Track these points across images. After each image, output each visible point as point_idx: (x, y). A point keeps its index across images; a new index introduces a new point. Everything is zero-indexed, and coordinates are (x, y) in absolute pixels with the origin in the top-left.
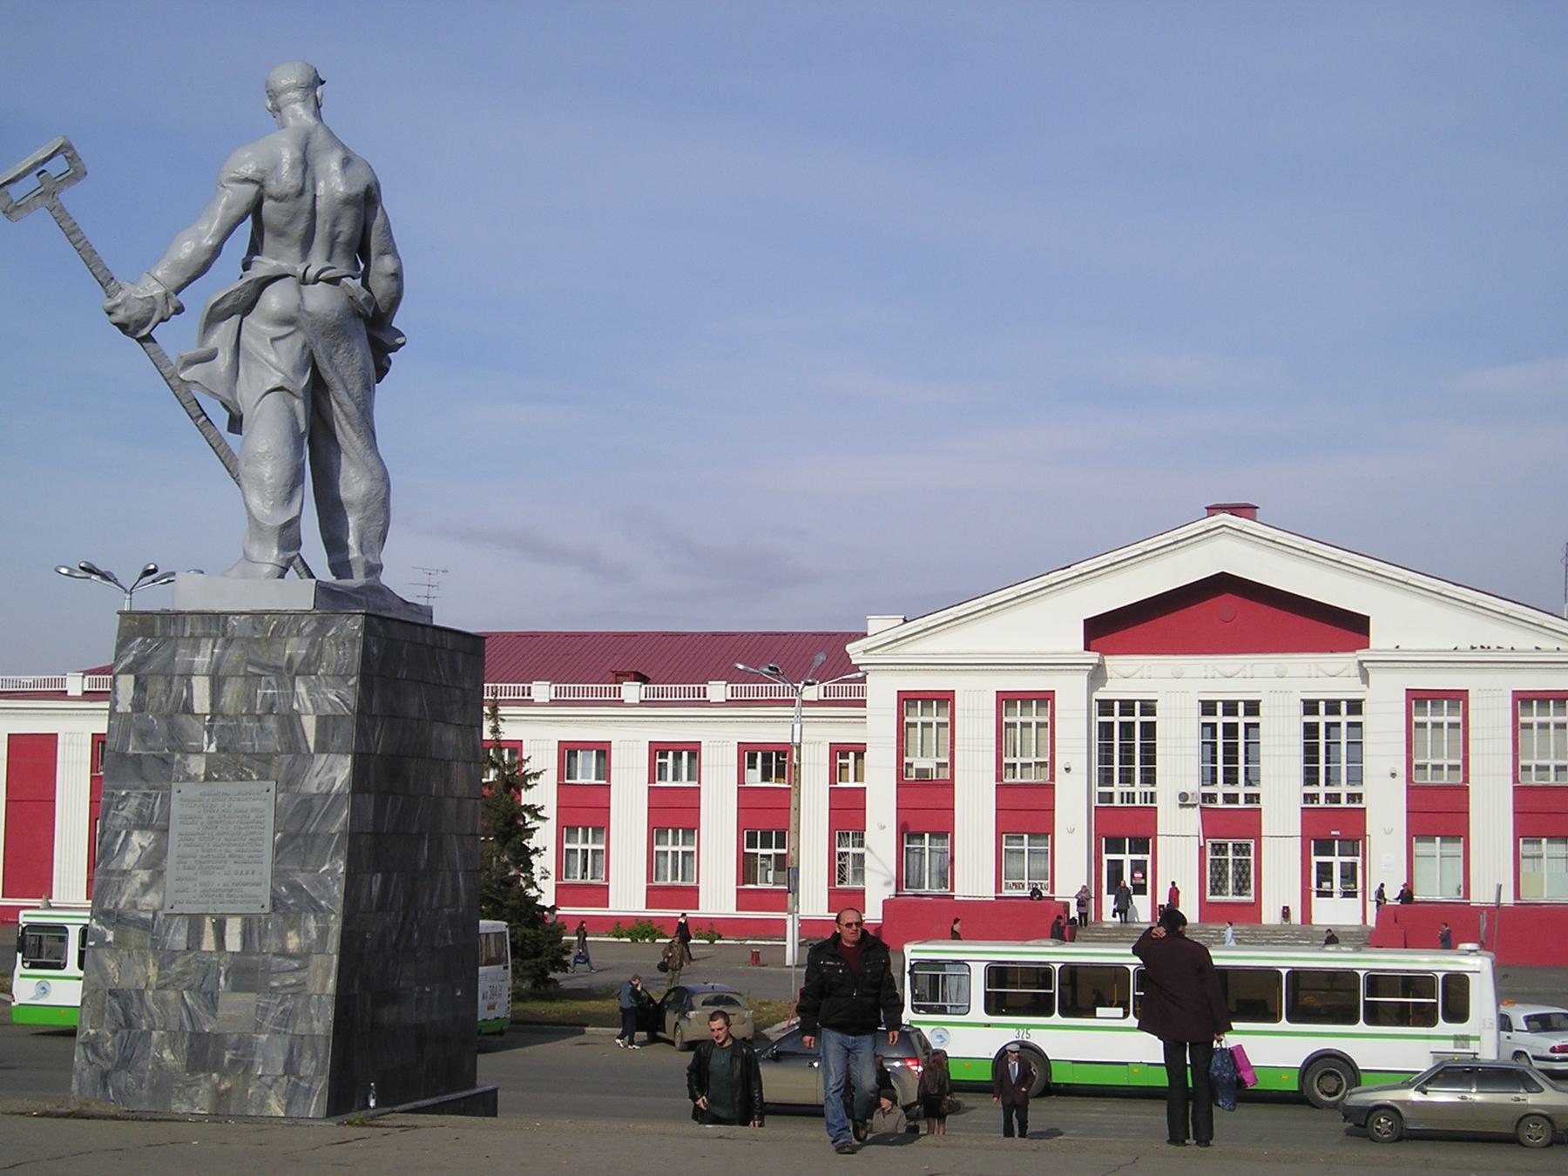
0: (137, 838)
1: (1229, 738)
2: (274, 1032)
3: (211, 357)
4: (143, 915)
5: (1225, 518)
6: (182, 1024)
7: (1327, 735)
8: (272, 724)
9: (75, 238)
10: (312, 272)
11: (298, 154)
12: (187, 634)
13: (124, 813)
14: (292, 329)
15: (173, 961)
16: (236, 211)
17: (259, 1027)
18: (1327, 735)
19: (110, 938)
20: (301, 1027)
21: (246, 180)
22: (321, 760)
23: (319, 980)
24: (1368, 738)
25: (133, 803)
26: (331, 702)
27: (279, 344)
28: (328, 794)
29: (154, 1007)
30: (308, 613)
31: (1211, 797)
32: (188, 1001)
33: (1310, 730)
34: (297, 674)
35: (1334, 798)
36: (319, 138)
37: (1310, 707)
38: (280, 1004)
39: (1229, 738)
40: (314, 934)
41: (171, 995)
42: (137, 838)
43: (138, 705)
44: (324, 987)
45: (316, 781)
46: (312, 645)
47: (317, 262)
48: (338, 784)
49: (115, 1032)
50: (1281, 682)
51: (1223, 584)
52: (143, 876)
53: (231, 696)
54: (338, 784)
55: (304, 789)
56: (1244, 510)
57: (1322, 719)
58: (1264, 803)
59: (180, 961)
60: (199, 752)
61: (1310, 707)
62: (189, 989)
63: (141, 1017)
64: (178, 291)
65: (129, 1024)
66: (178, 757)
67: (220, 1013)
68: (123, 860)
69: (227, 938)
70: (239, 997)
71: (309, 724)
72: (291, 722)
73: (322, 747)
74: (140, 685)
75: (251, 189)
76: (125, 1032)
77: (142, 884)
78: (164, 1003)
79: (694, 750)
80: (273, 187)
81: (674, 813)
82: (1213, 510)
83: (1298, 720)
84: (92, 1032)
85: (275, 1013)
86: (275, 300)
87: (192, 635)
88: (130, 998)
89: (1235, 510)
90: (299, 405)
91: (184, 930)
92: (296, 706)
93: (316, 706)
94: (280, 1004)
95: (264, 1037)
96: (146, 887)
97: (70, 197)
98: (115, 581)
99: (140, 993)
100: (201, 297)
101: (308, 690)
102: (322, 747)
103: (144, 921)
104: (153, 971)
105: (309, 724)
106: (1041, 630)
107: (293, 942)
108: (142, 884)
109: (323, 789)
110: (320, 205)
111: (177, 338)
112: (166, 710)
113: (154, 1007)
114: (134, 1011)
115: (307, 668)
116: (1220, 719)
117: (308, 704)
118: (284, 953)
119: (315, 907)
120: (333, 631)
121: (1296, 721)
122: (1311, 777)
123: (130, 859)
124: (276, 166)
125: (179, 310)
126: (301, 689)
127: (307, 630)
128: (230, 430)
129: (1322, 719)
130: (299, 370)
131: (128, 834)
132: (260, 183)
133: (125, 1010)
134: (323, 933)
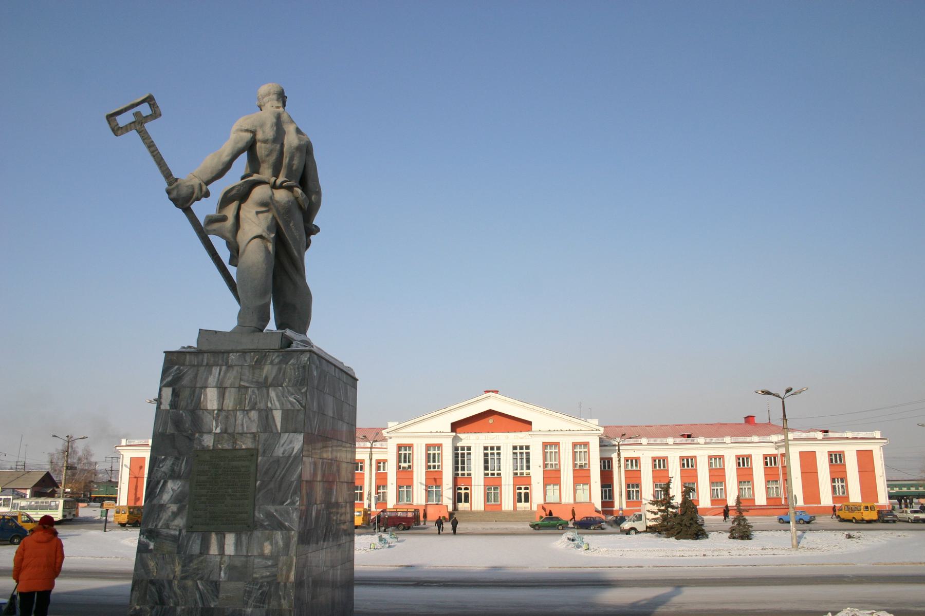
0: (170, 485)
1: (491, 455)
2: (255, 607)
3: (224, 219)
4: (172, 532)
5: (491, 394)
6: (196, 603)
7: (522, 454)
8: (254, 414)
9: (152, 149)
10: (279, 182)
11: (274, 120)
12: (205, 363)
13: (163, 469)
14: (263, 209)
15: (191, 561)
16: (241, 145)
17: (246, 604)
18: (522, 454)
19: (152, 546)
20: (274, 604)
21: (247, 131)
22: (285, 437)
23: (284, 572)
24: (502, 456)
25: (169, 463)
26: (291, 403)
27: (261, 215)
28: (289, 456)
29: (178, 591)
30: (275, 350)
31: (487, 474)
32: (200, 586)
33: (486, 455)
34: (270, 386)
35: (493, 474)
36: (284, 117)
37: (486, 448)
38: (259, 589)
39: (491, 455)
40: (281, 543)
41: (189, 583)
42: (170, 485)
43: (174, 405)
44: (288, 577)
45: (282, 450)
46: (280, 369)
47: (281, 179)
48: (295, 451)
49: (152, 608)
50: (506, 440)
51: (490, 413)
52: (174, 508)
53: (229, 403)
54: (295, 451)
55: (275, 454)
56: (496, 392)
57: (489, 452)
58: (472, 476)
59: (195, 562)
60: (210, 432)
61: (486, 448)
62: (201, 579)
63: (169, 597)
64: (208, 183)
65: (162, 602)
66: (197, 435)
67: (221, 595)
68: (161, 498)
69: (226, 547)
70: (233, 585)
71: (278, 415)
72: (266, 417)
73: (285, 430)
74: (175, 394)
75: (248, 136)
76: (159, 607)
77: (173, 513)
78: (184, 588)
79: (441, 445)
80: (260, 136)
81: (717, 477)
82: (487, 392)
83: (482, 452)
84: (138, 607)
85: (256, 594)
86: (259, 193)
87: (207, 365)
88: (164, 586)
89: (493, 392)
90: (271, 247)
91: (199, 542)
92: (269, 405)
93: (282, 404)
94: (259, 589)
95: (249, 610)
96: (175, 515)
97: (150, 127)
98: (167, 174)
99: (170, 582)
100: (218, 189)
101: (277, 396)
102: (285, 430)
103: (174, 536)
104: (178, 569)
105: (278, 415)
106: (443, 422)
107: (268, 549)
108: (173, 513)
109: (286, 454)
110: (285, 149)
111: (204, 209)
112: (191, 408)
113: (178, 591)
114: (166, 593)
115: (276, 384)
116: (518, 451)
117: (277, 404)
118: (262, 555)
119: (281, 526)
120: (292, 361)
121: (481, 452)
122: (486, 468)
123: (166, 497)
124: (262, 125)
125: (207, 194)
126: (273, 394)
127: (276, 361)
128: (230, 263)
129: (489, 452)
130: (269, 229)
131: (165, 483)
132: (254, 133)
133: (160, 592)
134: (287, 545)
